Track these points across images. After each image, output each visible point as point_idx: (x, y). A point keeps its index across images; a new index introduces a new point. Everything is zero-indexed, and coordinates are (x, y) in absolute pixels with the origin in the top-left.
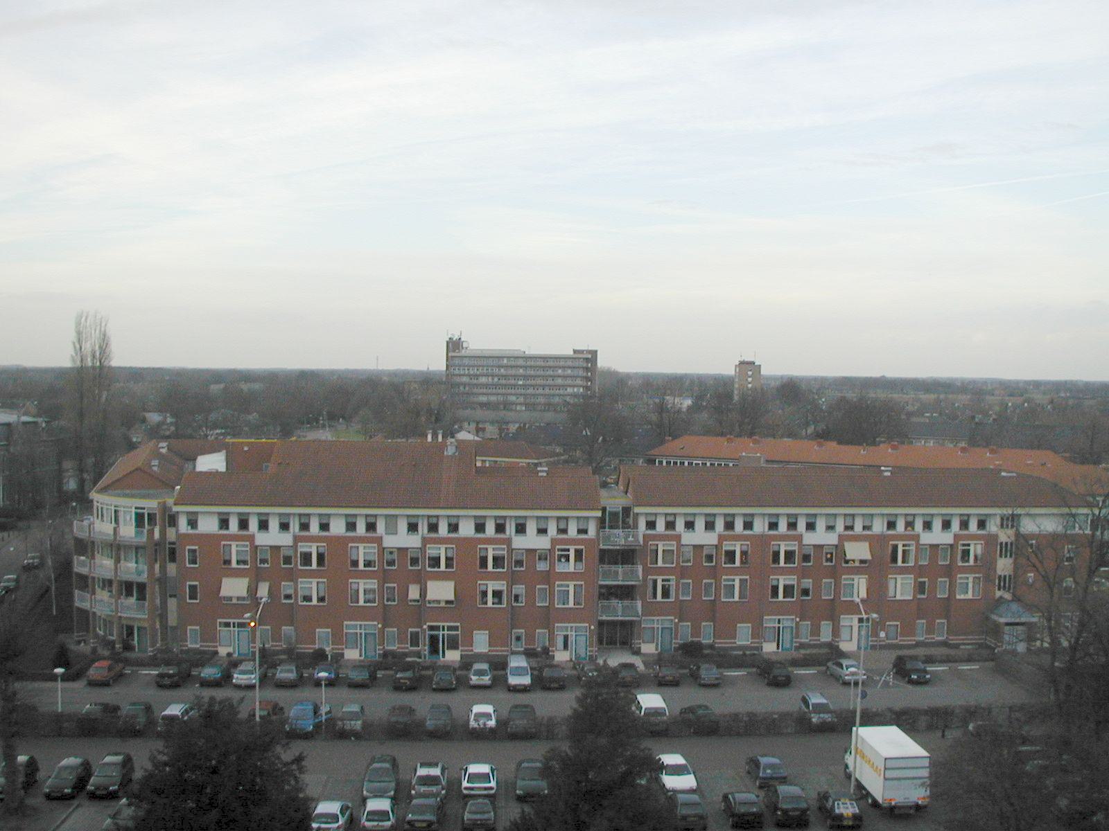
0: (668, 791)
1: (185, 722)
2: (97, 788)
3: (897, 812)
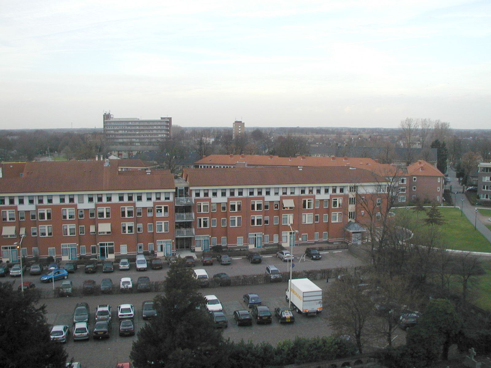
0: (210, 311)
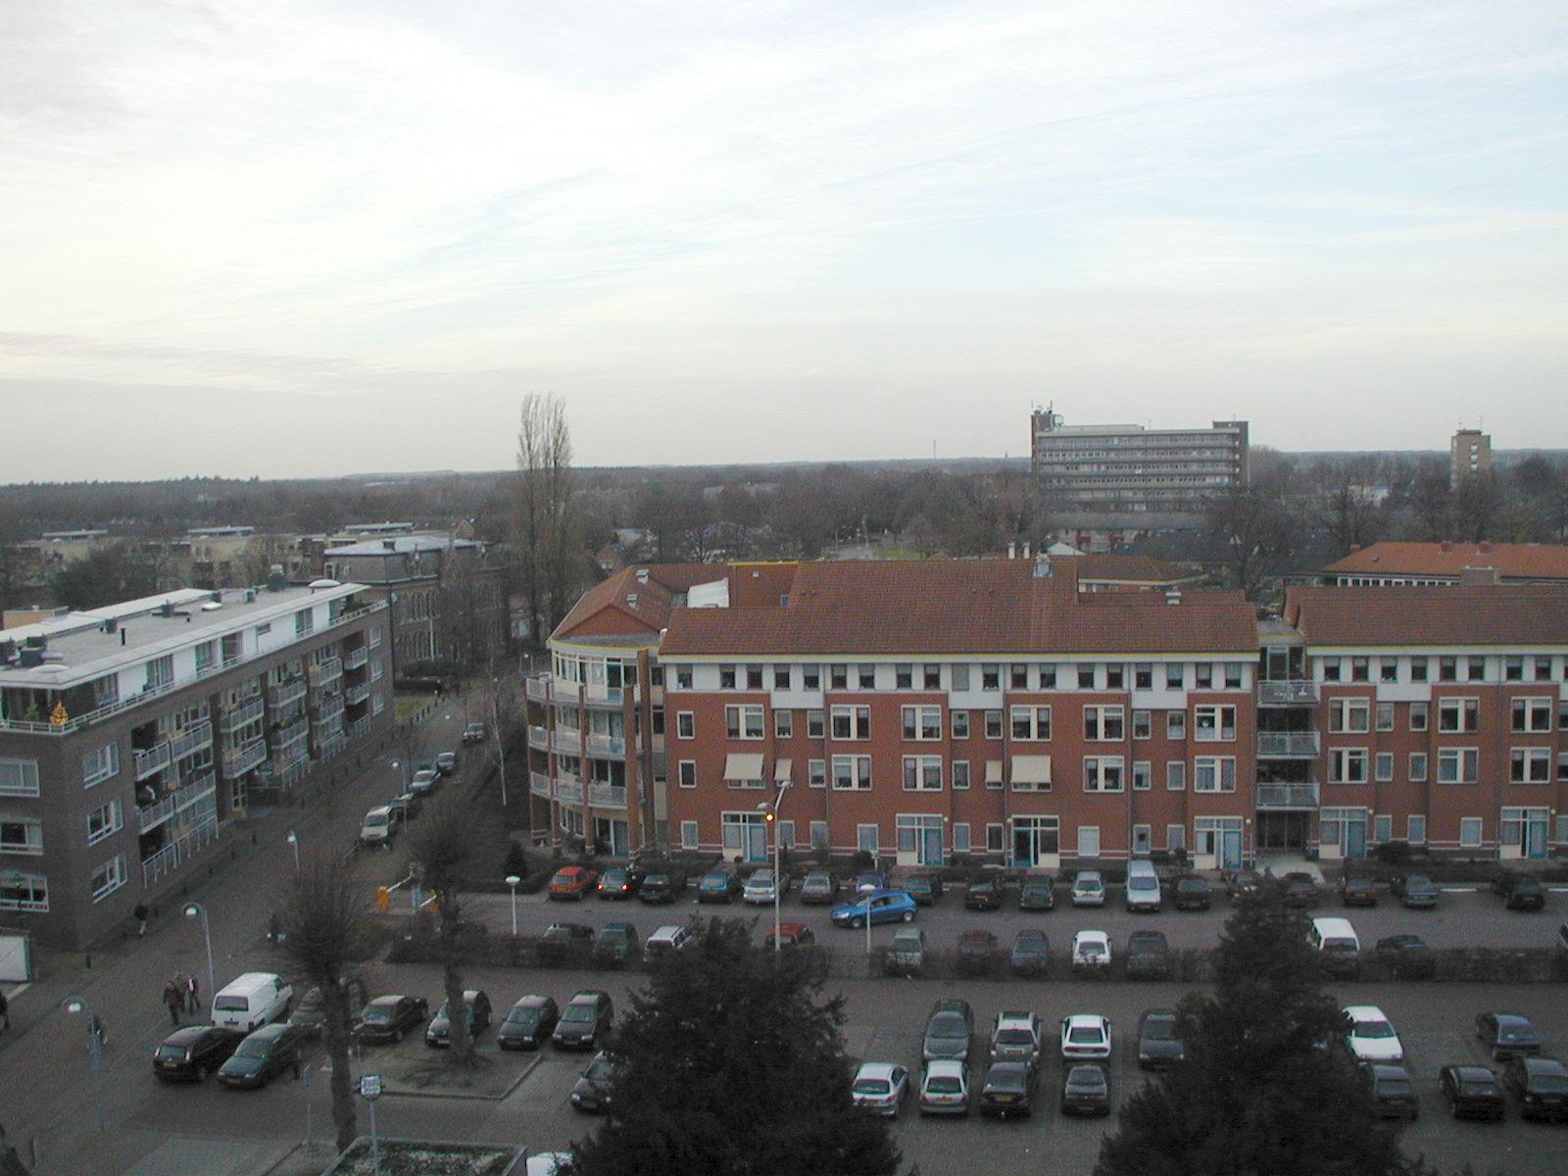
0: (1361, 1060)
1: (679, 953)
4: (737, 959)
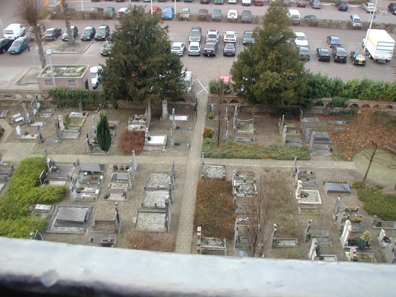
0: (297, 46)
1: (126, 14)
2: (98, 37)
3: (379, 61)
4: (141, 16)
